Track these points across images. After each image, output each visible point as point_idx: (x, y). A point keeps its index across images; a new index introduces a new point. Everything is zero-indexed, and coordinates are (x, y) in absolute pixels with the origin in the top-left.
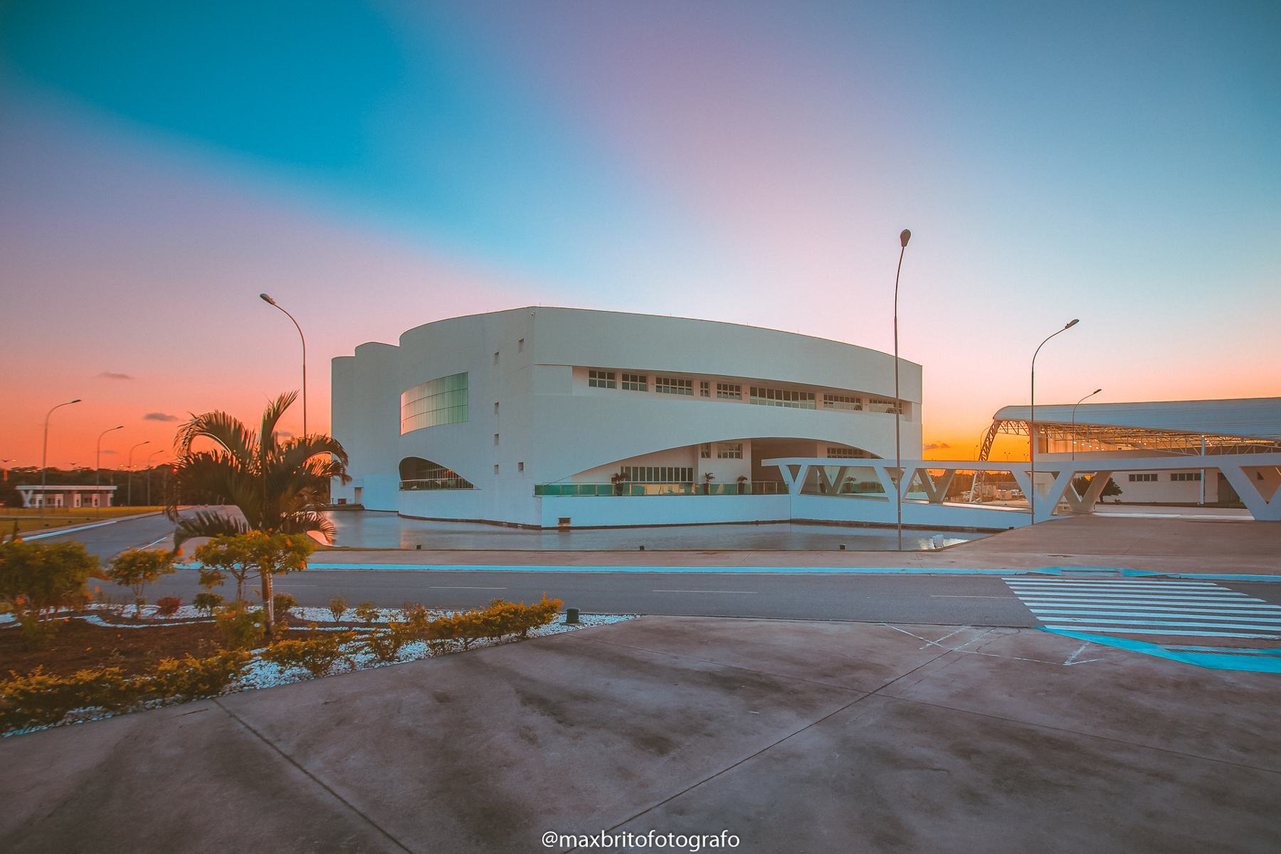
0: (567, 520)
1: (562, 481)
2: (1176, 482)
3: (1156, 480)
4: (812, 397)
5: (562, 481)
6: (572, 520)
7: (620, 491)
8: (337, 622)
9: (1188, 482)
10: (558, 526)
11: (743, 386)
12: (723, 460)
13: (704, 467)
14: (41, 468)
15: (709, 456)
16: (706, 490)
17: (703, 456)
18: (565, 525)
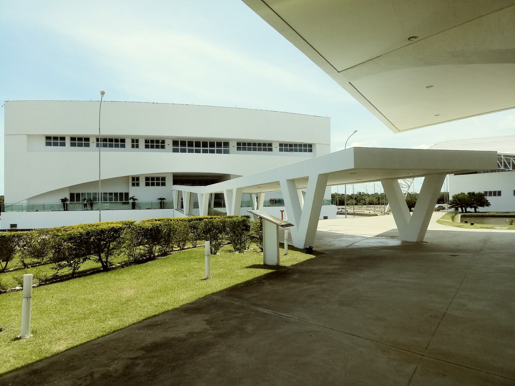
0: (15, 226)
1: (20, 203)
2: (499, 190)
3: (146, 148)
4: (175, 143)
5: (20, 203)
6: (18, 226)
7: (66, 208)
8: (73, 273)
9: (492, 191)
10: (10, 229)
11: (273, 143)
12: (150, 188)
13: (133, 192)
14: (373, 193)
15: (138, 185)
16: (134, 206)
17: (133, 185)
18: (14, 228)
